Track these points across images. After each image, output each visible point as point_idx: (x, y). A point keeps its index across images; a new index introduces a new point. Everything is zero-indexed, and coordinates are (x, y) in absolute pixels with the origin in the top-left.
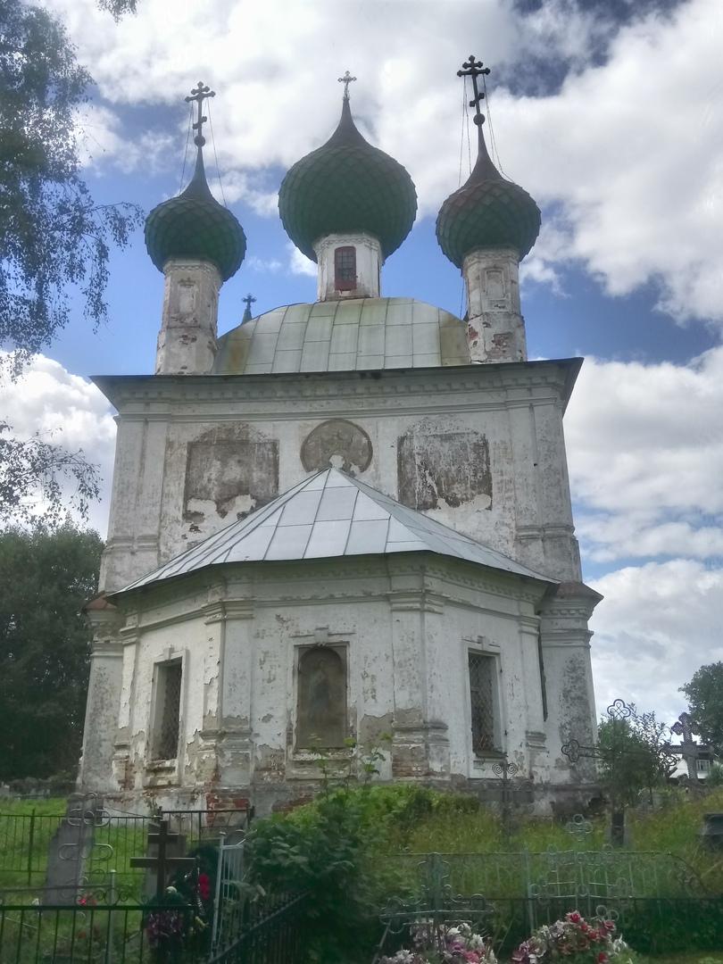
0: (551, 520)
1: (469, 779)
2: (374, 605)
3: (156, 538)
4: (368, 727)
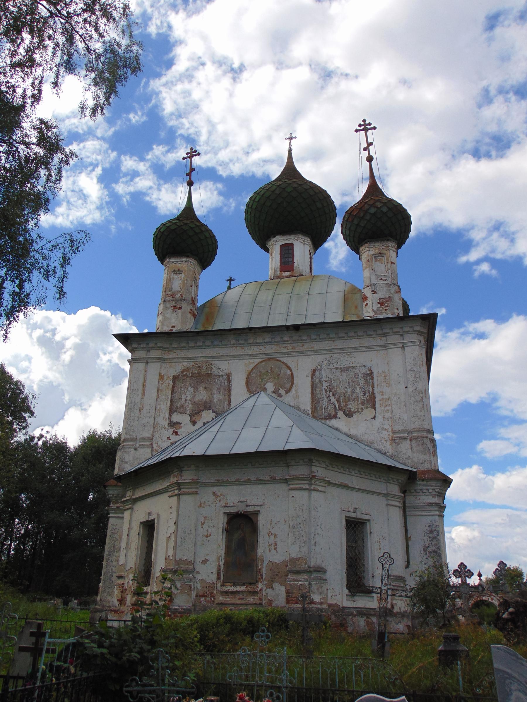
0: (417, 426)
1: (343, 607)
2: (277, 486)
3: (151, 439)
4: (271, 570)
